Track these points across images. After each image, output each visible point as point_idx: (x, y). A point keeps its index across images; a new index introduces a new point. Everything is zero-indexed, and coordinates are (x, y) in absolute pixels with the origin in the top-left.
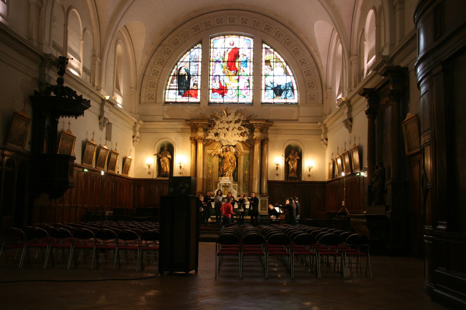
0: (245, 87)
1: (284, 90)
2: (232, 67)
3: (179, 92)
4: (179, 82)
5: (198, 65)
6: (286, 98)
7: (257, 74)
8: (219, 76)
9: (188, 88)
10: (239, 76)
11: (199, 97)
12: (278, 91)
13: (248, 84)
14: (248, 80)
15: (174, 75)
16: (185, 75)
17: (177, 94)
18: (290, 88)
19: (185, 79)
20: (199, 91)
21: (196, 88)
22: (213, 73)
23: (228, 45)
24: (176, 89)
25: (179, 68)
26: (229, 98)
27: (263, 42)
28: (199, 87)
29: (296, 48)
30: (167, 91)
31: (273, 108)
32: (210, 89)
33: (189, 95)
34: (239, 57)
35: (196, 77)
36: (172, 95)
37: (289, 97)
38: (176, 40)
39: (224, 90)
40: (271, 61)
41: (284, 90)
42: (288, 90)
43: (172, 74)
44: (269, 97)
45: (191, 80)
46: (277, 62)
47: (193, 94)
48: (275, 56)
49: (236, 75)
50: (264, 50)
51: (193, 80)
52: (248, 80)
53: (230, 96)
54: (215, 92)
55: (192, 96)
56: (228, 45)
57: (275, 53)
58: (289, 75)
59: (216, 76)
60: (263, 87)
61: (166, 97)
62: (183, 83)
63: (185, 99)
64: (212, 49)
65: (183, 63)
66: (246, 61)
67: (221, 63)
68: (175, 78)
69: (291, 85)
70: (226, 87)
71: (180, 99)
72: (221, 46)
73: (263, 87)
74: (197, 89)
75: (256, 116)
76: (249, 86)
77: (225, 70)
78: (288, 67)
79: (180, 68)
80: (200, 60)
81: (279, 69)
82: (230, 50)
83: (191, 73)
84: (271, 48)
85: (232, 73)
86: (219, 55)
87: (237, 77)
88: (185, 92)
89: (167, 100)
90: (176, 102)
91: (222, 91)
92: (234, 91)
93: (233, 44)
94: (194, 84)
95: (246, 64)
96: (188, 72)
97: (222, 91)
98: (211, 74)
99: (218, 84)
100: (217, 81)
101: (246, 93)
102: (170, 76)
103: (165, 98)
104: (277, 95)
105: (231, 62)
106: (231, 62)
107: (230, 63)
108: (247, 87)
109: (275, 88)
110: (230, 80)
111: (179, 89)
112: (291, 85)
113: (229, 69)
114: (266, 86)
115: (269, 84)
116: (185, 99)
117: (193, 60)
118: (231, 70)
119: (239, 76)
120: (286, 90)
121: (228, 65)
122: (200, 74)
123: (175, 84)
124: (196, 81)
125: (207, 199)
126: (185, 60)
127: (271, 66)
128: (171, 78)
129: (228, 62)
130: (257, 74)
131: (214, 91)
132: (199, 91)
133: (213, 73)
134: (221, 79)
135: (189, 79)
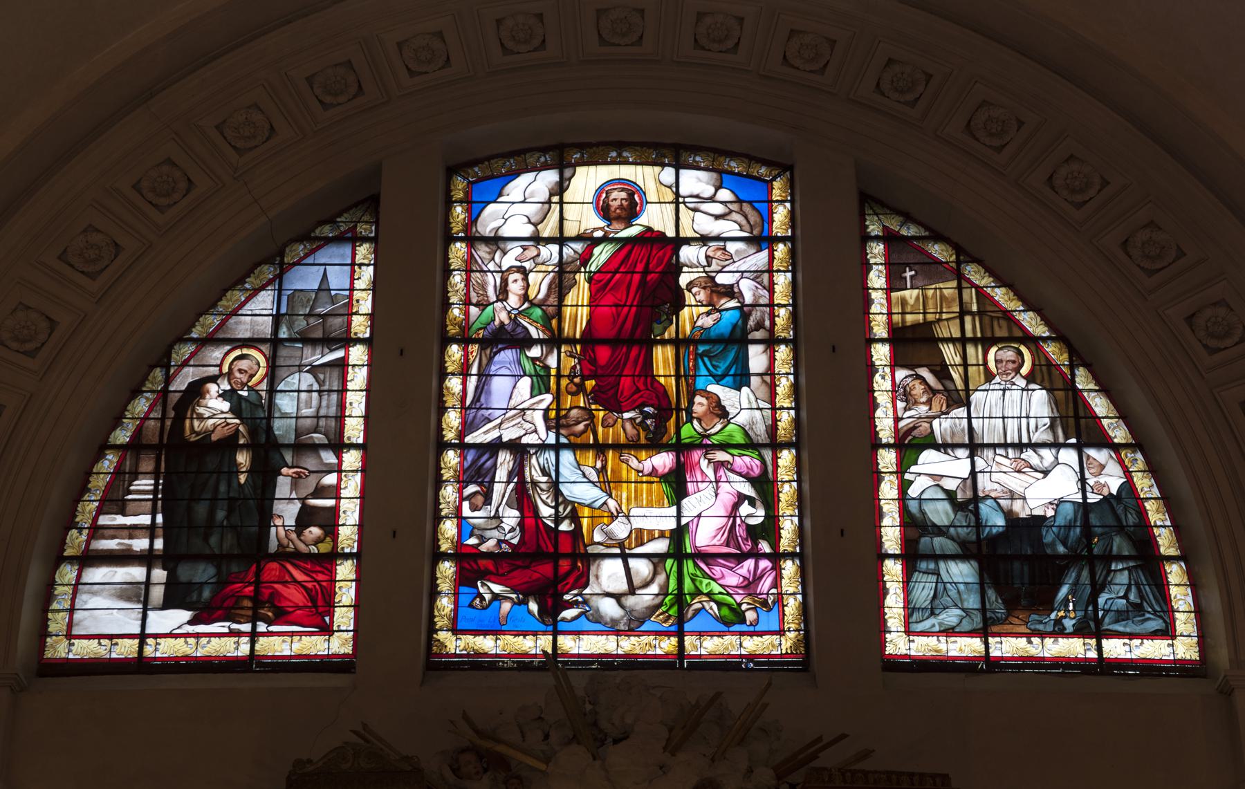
0: (731, 539)
1: (1073, 558)
2: (626, 382)
3: (169, 585)
4: (168, 501)
5: (342, 365)
6: (1092, 628)
7: (834, 444)
8: (518, 449)
9: (254, 547)
10: (681, 448)
11: (344, 618)
12: (1019, 565)
13: (755, 515)
14: (765, 486)
15: (136, 446)
16: (230, 444)
17: (157, 593)
18: (1119, 544)
19: (234, 469)
20: (345, 570)
21: (325, 548)
22: (467, 427)
23: (583, 217)
24: (147, 559)
25: (180, 384)
26: (609, 618)
27: (868, 201)
28: (347, 535)
29: (1151, 224)
30: (68, 573)
31: (1184, 486)
32: (439, 556)
33: (257, 602)
34: (678, 302)
35: (329, 457)
36: (108, 613)
37: (1121, 616)
38: (170, 162)
39: (556, 557)
40: (942, 331)
41: (1073, 558)
42: (1108, 558)
43: (122, 436)
44: (951, 617)
45: (283, 486)
46: (986, 342)
47: (294, 595)
48: (970, 295)
49: (655, 445)
50: (877, 250)
51: (296, 482)
52: (765, 486)
53: (609, 608)
54: (486, 576)
55: (281, 616)
56: (583, 217)
57: (974, 273)
58: (1104, 442)
59: (496, 446)
60: (891, 537)
61: (57, 623)
62: (220, 534)
63: (222, 642)
64: (459, 250)
65: (216, 354)
66: (738, 339)
67: (535, 352)
68: (147, 465)
69: (1132, 519)
70: (577, 532)
71: (173, 632)
72: (534, 222)
73: (891, 537)
74: (335, 556)
75: (866, 754)
76: (770, 528)
77: (568, 401)
78: (1083, 381)
79: (196, 391)
80: (360, 326)
81: (1012, 405)
82: (602, 254)
83: (281, 427)
84: (937, 237)
85: (627, 422)
86: (515, 288)
87: (663, 461)
88: (222, 582)
89: (59, 649)
90: (140, 665)
91: (549, 564)
92: (642, 568)
93: (631, 212)
94: (306, 517)
95: (743, 360)
96: (254, 412)
97: (546, 569)
98: (450, 436)
99: (511, 517)
100: (501, 489)
101: (750, 585)
102: (100, 456)
103: (44, 633)
104: (1012, 604)
105: (614, 342)
106: (614, 342)
107: (603, 353)
108: (754, 533)
109: (995, 540)
110: (608, 483)
111: (168, 559)
112: (1132, 519)
113: (598, 396)
114: (914, 524)
115: (940, 513)
116: (222, 642)
117: (301, 323)
118: (614, 406)
119: (681, 448)
120: (1092, 560)
121: (589, 366)
122: (354, 430)
123: (139, 518)
124: (320, 492)
125: (877, 215)
126: (243, 327)
127: (942, 372)
128: (109, 462)
129: (589, 339)
130: (834, 444)
131: (473, 567)
132: (345, 570)
133: (467, 427)
134: (533, 472)
135: (265, 473)
